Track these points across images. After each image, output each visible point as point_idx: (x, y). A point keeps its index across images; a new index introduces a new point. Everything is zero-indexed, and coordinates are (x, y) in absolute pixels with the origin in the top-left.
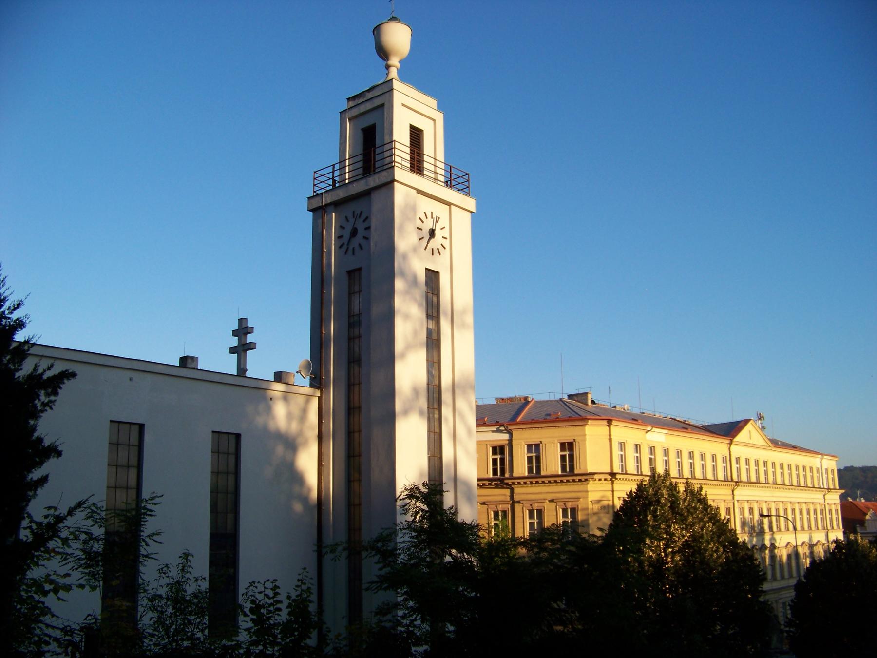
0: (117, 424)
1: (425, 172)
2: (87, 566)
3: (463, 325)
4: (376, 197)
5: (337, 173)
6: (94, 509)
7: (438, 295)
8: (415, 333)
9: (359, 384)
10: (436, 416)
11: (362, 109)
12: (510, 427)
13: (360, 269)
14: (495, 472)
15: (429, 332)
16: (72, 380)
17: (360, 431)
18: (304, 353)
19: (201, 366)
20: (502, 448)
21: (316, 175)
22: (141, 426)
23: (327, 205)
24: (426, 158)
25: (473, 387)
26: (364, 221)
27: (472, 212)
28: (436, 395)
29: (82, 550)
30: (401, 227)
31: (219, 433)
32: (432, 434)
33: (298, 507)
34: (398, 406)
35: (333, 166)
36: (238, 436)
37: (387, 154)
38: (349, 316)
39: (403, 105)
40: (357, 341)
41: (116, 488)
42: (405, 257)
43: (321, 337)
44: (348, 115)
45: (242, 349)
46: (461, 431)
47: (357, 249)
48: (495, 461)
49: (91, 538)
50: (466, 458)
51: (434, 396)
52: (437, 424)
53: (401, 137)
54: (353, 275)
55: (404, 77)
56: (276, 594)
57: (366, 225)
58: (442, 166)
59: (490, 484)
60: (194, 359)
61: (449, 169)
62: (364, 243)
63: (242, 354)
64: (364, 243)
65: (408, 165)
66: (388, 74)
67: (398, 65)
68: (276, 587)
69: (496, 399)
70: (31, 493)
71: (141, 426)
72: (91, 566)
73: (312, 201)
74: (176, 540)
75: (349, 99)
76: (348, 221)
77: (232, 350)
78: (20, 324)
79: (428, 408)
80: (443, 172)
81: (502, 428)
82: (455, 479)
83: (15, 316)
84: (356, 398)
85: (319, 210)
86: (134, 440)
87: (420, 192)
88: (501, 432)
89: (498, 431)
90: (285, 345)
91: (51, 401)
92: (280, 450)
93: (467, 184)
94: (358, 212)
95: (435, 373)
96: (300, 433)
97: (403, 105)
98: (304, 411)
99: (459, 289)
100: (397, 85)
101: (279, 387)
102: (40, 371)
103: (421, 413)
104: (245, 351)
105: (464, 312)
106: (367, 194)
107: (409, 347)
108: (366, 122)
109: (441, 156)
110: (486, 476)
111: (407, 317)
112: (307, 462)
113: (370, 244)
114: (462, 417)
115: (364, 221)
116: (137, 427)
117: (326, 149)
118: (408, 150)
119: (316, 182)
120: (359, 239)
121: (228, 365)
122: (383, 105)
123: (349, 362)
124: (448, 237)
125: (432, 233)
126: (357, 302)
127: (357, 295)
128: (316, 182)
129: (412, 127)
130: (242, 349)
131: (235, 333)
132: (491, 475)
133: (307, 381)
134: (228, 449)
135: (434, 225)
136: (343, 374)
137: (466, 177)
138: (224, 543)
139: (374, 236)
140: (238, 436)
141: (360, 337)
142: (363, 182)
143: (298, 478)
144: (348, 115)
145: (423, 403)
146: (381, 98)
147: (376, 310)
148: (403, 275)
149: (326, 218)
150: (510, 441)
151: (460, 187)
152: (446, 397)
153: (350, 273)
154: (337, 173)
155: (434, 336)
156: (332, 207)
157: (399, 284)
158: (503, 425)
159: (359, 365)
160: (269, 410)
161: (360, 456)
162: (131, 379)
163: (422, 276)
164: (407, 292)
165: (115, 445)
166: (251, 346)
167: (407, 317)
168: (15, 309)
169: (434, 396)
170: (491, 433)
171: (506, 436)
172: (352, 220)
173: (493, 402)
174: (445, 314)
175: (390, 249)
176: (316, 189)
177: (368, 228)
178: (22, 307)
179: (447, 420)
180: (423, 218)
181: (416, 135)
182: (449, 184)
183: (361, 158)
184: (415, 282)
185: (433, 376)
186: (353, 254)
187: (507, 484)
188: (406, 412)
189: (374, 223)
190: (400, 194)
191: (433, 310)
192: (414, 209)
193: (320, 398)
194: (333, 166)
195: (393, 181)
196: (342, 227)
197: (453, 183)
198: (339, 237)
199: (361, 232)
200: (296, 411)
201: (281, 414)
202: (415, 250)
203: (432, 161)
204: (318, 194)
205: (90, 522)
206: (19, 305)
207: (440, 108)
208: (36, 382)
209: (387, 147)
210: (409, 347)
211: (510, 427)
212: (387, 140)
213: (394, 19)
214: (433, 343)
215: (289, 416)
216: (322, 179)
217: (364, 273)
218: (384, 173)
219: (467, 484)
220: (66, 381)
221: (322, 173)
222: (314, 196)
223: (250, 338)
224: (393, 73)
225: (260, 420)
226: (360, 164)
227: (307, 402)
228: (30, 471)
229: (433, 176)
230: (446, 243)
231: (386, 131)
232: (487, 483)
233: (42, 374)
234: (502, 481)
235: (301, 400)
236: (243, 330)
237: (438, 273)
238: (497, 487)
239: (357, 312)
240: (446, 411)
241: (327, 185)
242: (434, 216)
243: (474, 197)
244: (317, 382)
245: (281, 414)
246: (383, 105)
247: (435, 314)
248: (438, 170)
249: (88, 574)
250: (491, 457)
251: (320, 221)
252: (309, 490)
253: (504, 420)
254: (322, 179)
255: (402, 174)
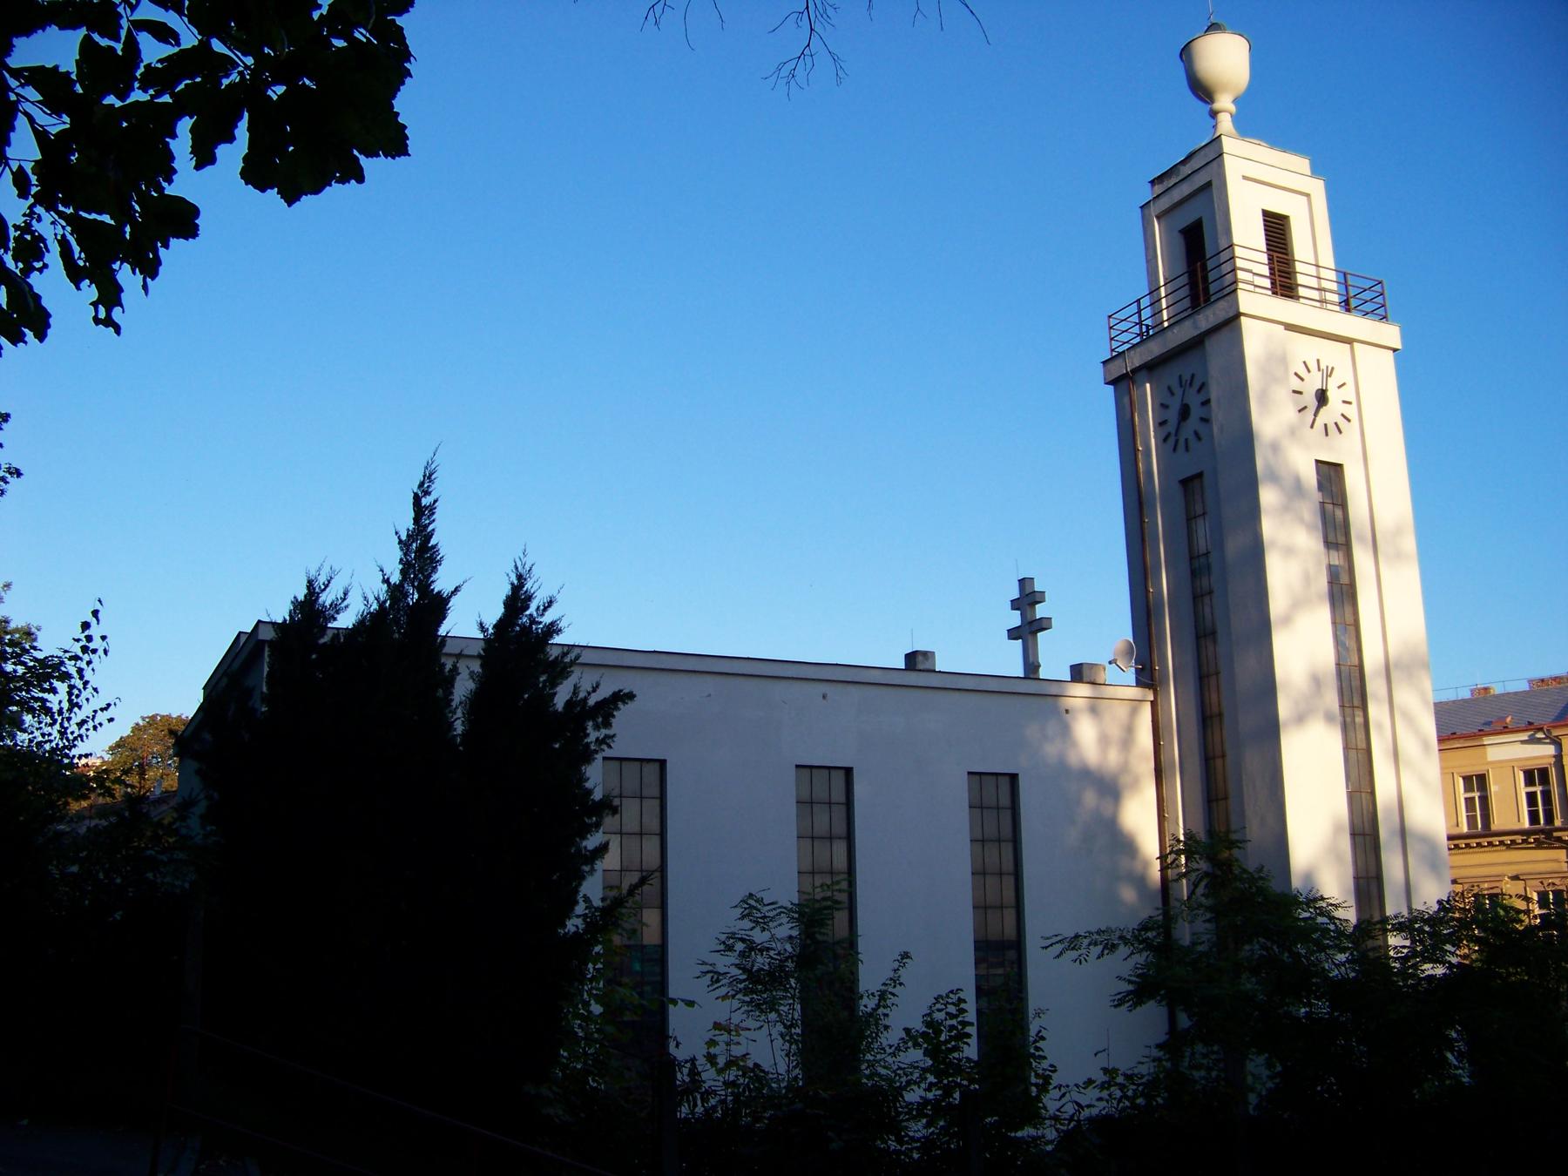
0: (617, 763)
1: (1302, 291)
2: (746, 991)
3: (1399, 556)
4: (1213, 346)
5: (1146, 314)
6: (752, 902)
7: (1343, 505)
8: (1307, 579)
9: (1217, 673)
10: (1359, 720)
11: (1177, 195)
12: (1555, 733)
13: (1200, 475)
14: (1533, 817)
15: (1333, 575)
16: (631, 705)
17: (1223, 756)
18: (1122, 630)
19: (940, 666)
20: (1544, 773)
21: (1113, 322)
22: (848, 771)
23: (1134, 371)
24: (1299, 267)
25: (1426, 666)
26: (1199, 391)
27: (1395, 350)
28: (1356, 683)
29: (736, 966)
30: (1264, 395)
31: (980, 774)
32: (1353, 754)
33: (1128, 894)
34: (1284, 708)
35: (1138, 301)
36: (1014, 778)
37: (1226, 268)
38: (1191, 559)
39: (1245, 178)
40: (1207, 600)
41: (813, 873)
42: (1275, 447)
43: (1147, 597)
44: (1154, 210)
45: (1028, 630)
46: (1408, 745)
47: (1193, 442)
48: (1531, 798)
49: (752, 949)
50: (1420, 793)
51: (1352, 689)
52: (1361, 735)
53: (1248, 238)
54: (1190, 485)
55: (1245, 128)
56: (963, 1011)
57: (1202, 398)
58: (1332, 275)
59: (1524, 841)
60: (928, 655)
61: (1344, 278)
62: (1201, 428)
63: (1030, 638)
64: (1201, 428)
65: (1267, 283)
66: (1215, 127)
67: (1233, 108)
68: (961, 1000)
69: (1530, 681)
70: (586, 868)
71: (848, 771)
72: (753, 991)
73: (1110, 366)
74: (914, 953)
75: (1152, 182)
76: (1172, 394)
77: (1013, 634)
78: (552, 629)
79: (1342, 706)
80: (1334, 286)
81: (1540, 735)
82: (1403, 832)
83: (547, 618)
84: (1214, 697)
85: (1122, 383)
86: (838, 795)
87: (1290, 327)
88: (1539, 741)
89: (1532, 741)
90: (1093, 619)
91: (607, 737)
92: (1090, 798)
93: (1379, 300)
94: (1186, 377)
95: (1352, 644)
96: (1125, 767)
97: (1245, 178)
98: (1129, 730)
99: (1383, 491)
100: (1230, 145)
101: (1081, 690)
102: (582, 695)
103: (1329, 718)
104: (1034, 633)
105: (1398, 532)
106: (1197, 343)
107: (1297, 604)
108: (1185, 218)
109: (1327, 259)
110: (1516, 827)
111: (1289, 551)
112: (1140, 818)
113: (1211, 430)
114: (1410, 720)
115: (1199, 391)
116: (842, 773)
117: (1126, 274)
118: (1264, 258)
119: (1114, 333)
120: (1193, 423)
121: (1009, 660)
122: (1209, 185)
123: (1198, 638)
124: (1352, 398)
125: (1322, 397)
126: (1201, 533)
127: (1200, 521)
128: (1114, 333)
129: (1266, 213)
130: (1028, 630)
131: (1015, 605)
132: (1526, 824)
133: (1130, 676)
134: (998, 802)
135: (1325, 383)
136: (1189, 658)
137: (1378, 288)
138: (1000, 957)
139: (1218, 414)
140: (1014, 778)
141: (1211, 592)
142: (1188, 323)
143: (1125, 845)
144: (1154, 210)
145: (1331, 699)
146: (1202, 172)
147: (1234, 545)
148: (1274, 478)
149: (1135, 393)
150: (1559, 757)
151: (1368, 307)
152: (1375, 686)
153: (1185, 483)
154: (1146, 314)
155: (1344, 579)
156: (1144, 373)
157: (1268, 497)
158: (1541, 729)
159: (1215, 642)
160: (1066, 731)
161: (1226, 798)
162: (824, 697)
163: (1310, 476)
164: (1286, 509)
165: (806, 804)
166: (1043, 625)
167: (1289, 551)
168: (545, 609)
169: (1352, 689)
170: (1519, 746)
171: (1550, 750)
172: (1178, 391)
173: (1524, 687)
174: (1362, 539)
175: (1245, 438)
176: (1115, 344)
177: (1206, 402)
178: (555, 606)
179: (1380, 726)
180: (1302, 372)
181: (1276, 228)
182: (1346, 306)
183: (1184, 280)
184: (1298, 488)
185: (1347, 649)
186: (1187, 449)
187: (1559, 839)
188: (1300, 719)
189: (1214, 393)
190: (1256, 340)
191: (1336, 531)
192: (1283, 360)
193: (1154, 704)
194: (1138, 301)
195: (1238, 315)
196: (1164, 406)
197: (1353, 303)
198: (1161, 424)
199: (1196, 412)
200: (1115, 731)
201: (1088, 738)
202: (1293, 432)
203: (1312, 270)
204: (1120, 354)
205: (747, 924)
206: (550, 603)
207: (1316, 171)
208: (580, 712)
209: (1224, 256)
210: (1297, 604)
211: (1555, 733)
212: (1223, 244)
213: (1214, 27)
214: (1342, 593)
215: (1104, 740)
216: (1124, 326)
217: (1207, 479)
218: (1222, 304)
219: (1426, 840)
220: (620, 705)
221: (1121, 316)
222: (1112, 358)
223: (1041, 611)
224: (1225, 123)
225: (1051, 750)
226: (1185, 291)
227: (1134, 713)
228: (584, 838)
229: (1315, 295)
230: (1351, 411)
231: (1219, 227)
232: (1519, 839)
233: (585, 699)
234: (1548, 834)
235: (1122, 711)
236: (1027, 598)
237: (1340, 466)
238: (1539, 845)
239: (1203, 550)
240: (1377, 711)
241: (1131, 337)
242: (1323, 366)
243: (1394, 322)
244: (1147, 676)
245: (1088, 738)
246: (1209, 185)
247: (1341, 540)
248: (1325, 284)
249: (748, 1003)
250: (1523, 790)
251: (1126, 400)
252: (1146, 864)
253: (1545, 721)
254: (1124, 326)
255: (1254, 299)
